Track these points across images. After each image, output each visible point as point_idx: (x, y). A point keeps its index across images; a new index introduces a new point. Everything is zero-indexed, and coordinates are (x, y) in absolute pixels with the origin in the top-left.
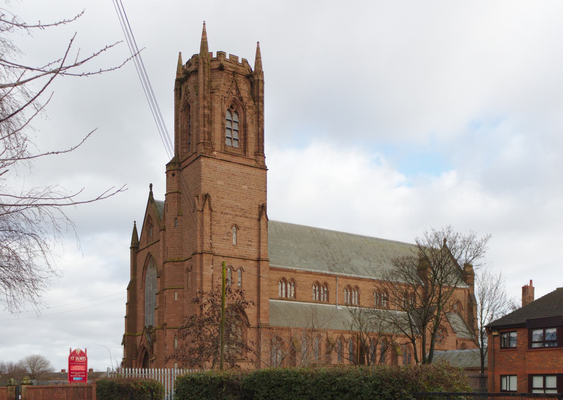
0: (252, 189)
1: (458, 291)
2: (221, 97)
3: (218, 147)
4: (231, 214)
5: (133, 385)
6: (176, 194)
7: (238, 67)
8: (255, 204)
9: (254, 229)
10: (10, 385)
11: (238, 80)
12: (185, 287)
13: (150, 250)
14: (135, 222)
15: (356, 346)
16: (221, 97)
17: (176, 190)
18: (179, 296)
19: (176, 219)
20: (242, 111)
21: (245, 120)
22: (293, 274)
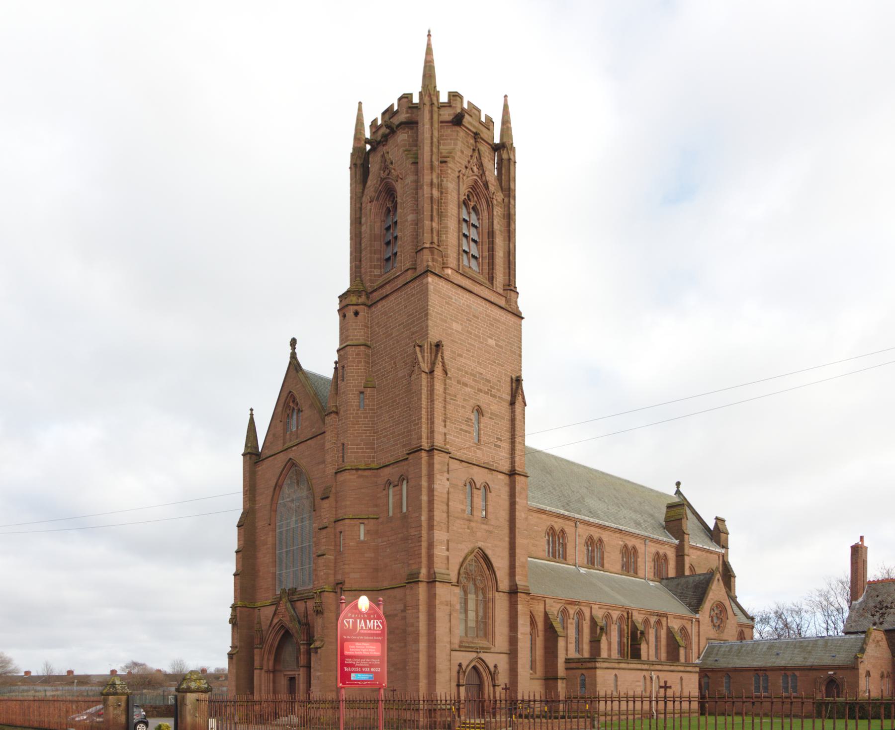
0: (501, 347)
3: (452, 261)
4: (472, 387)
6: (362, 348)
9: (503, 418)
10: (115, 694)
13: (291, 455)
15: (626, 631)
17: (362, 342)
18: (367, 532)
19: (362, 393)
20: (485, 208)
21: (492, 224)
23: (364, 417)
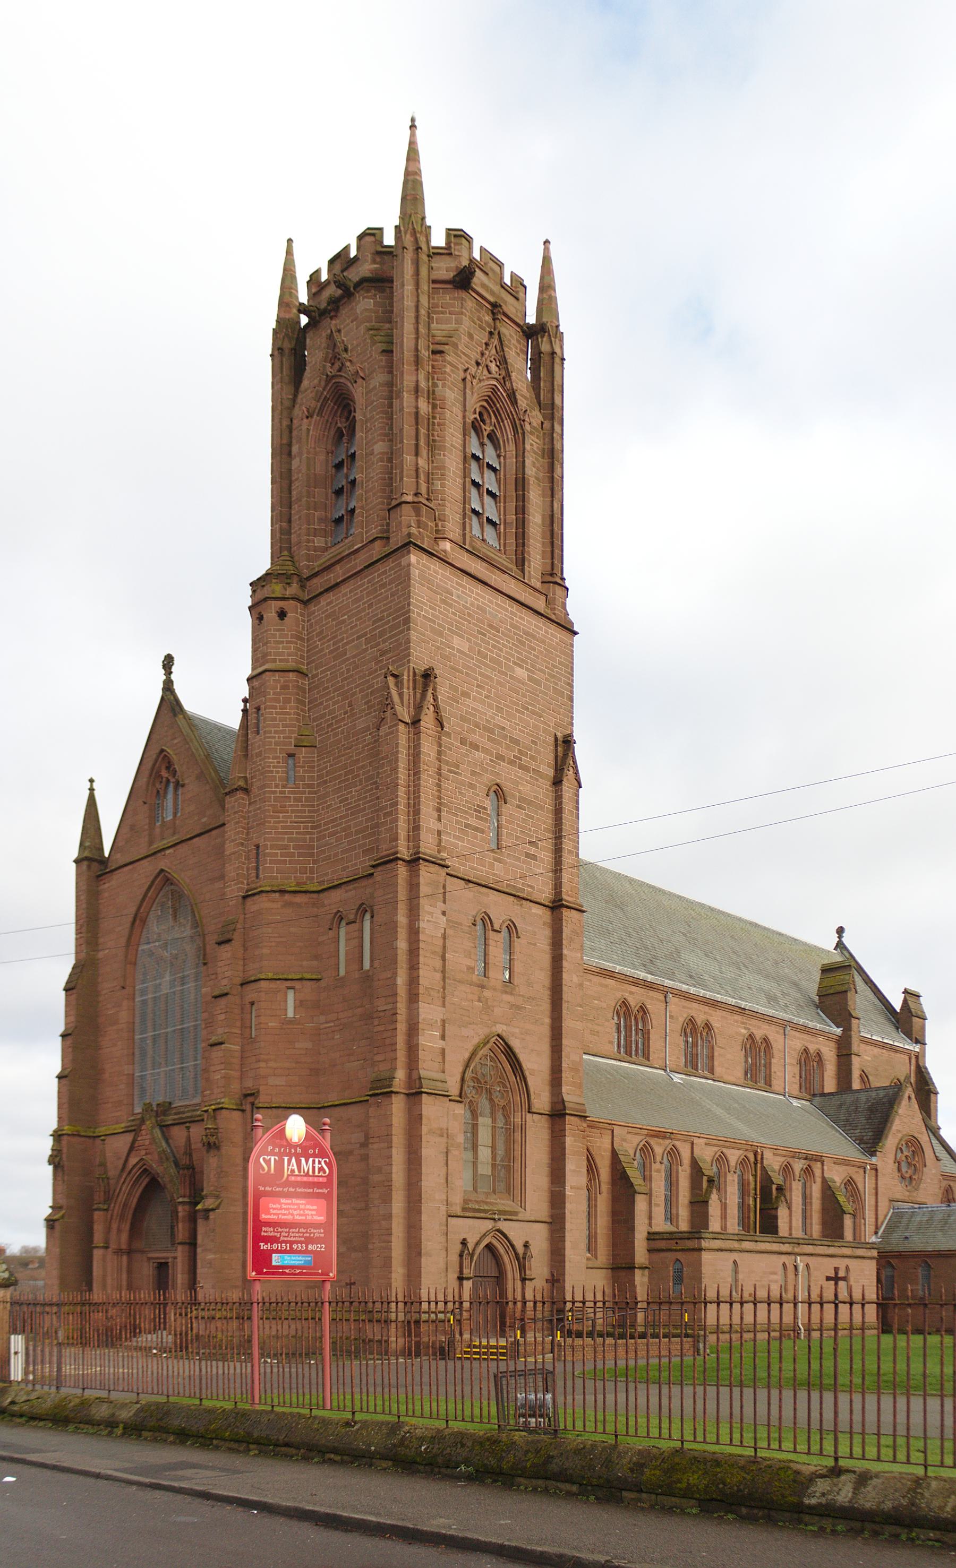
0: (537, 682)
1: (898, 1055)
4: (486, 751)
8: (545, 730)
9: (542, 808)
13: (163, 863)
18: (300, 1004)
19: (291, 755)
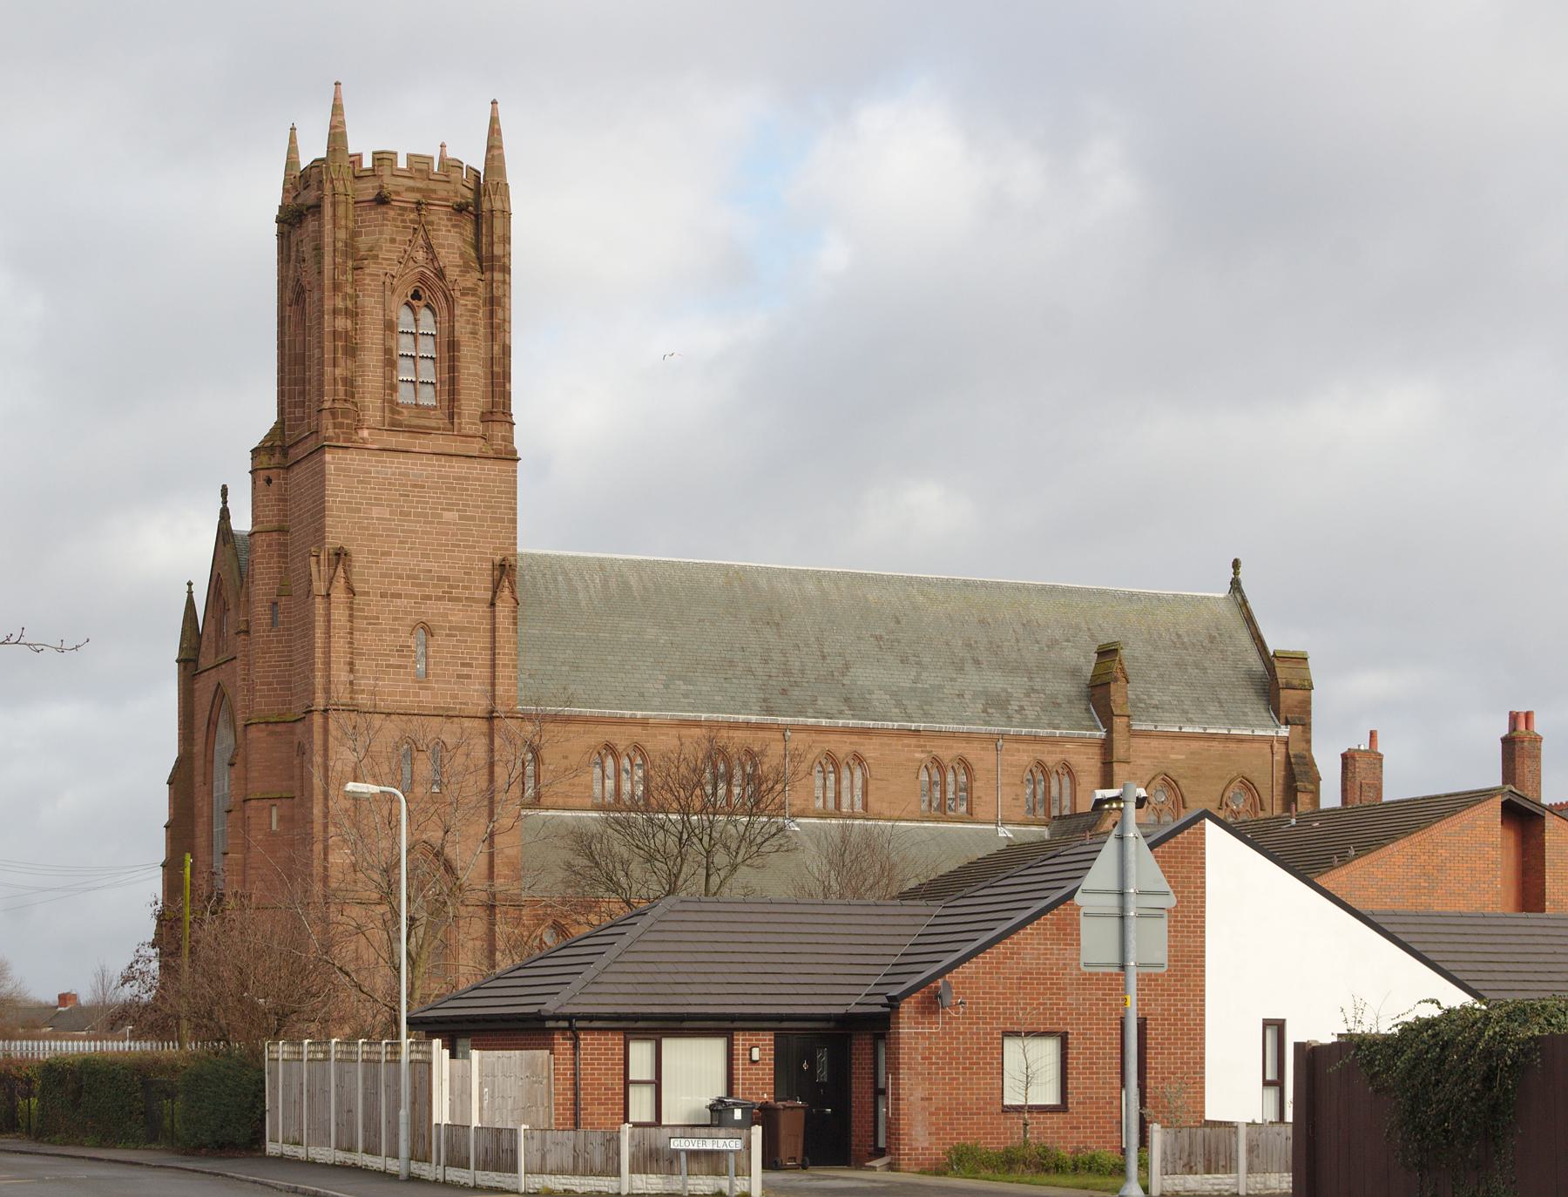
0: (473, 518)
2: (382, 278)
3: (373, 410)
4: (408, 596)
5: (14, 1071)
7: (432, 185)
8: (480, 559)
9: (477, 630)
11: (431, 223)
12: (297, 794)
14: (190, 584)
16: (382, 278)
18: (281, 819)
19: (275, 604)
22: (638, 730)
23: (279, 642)
